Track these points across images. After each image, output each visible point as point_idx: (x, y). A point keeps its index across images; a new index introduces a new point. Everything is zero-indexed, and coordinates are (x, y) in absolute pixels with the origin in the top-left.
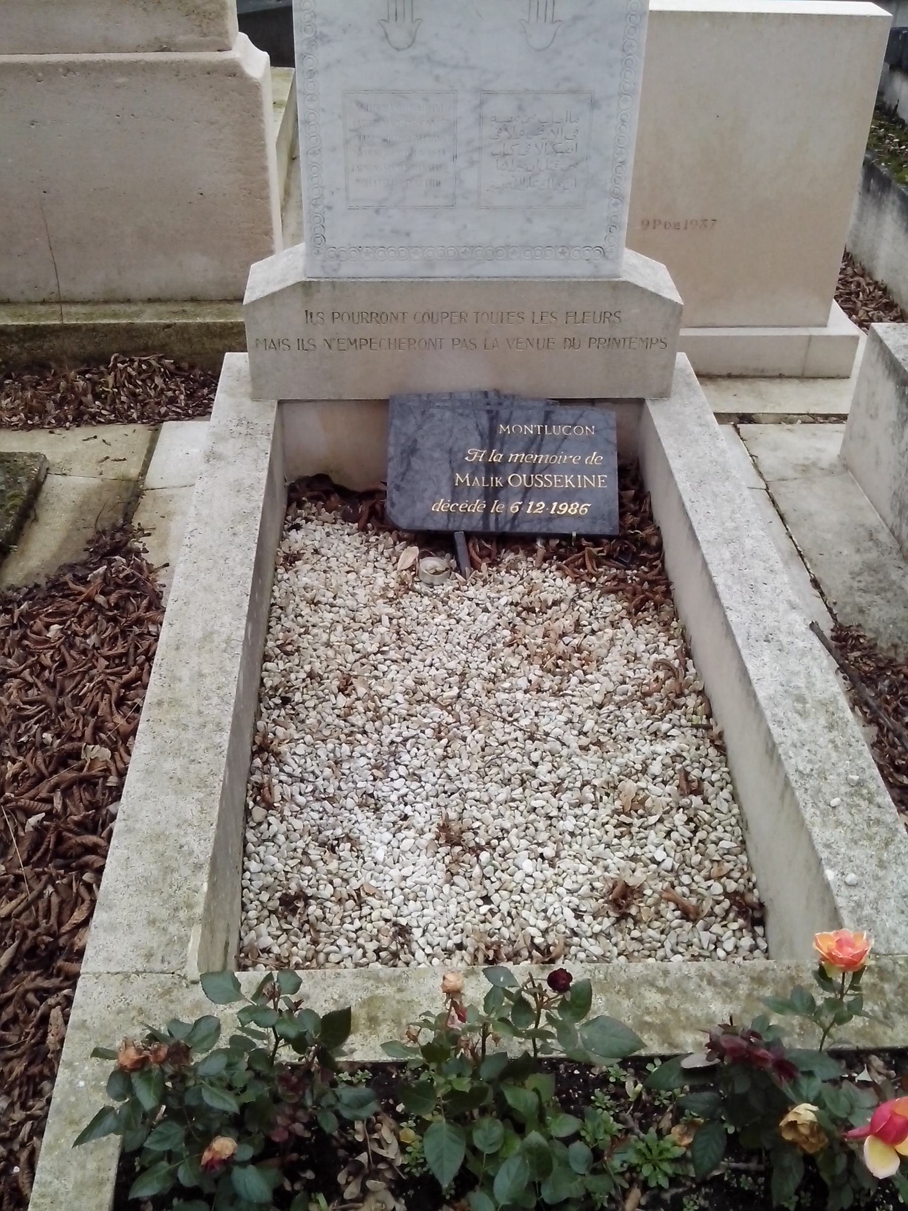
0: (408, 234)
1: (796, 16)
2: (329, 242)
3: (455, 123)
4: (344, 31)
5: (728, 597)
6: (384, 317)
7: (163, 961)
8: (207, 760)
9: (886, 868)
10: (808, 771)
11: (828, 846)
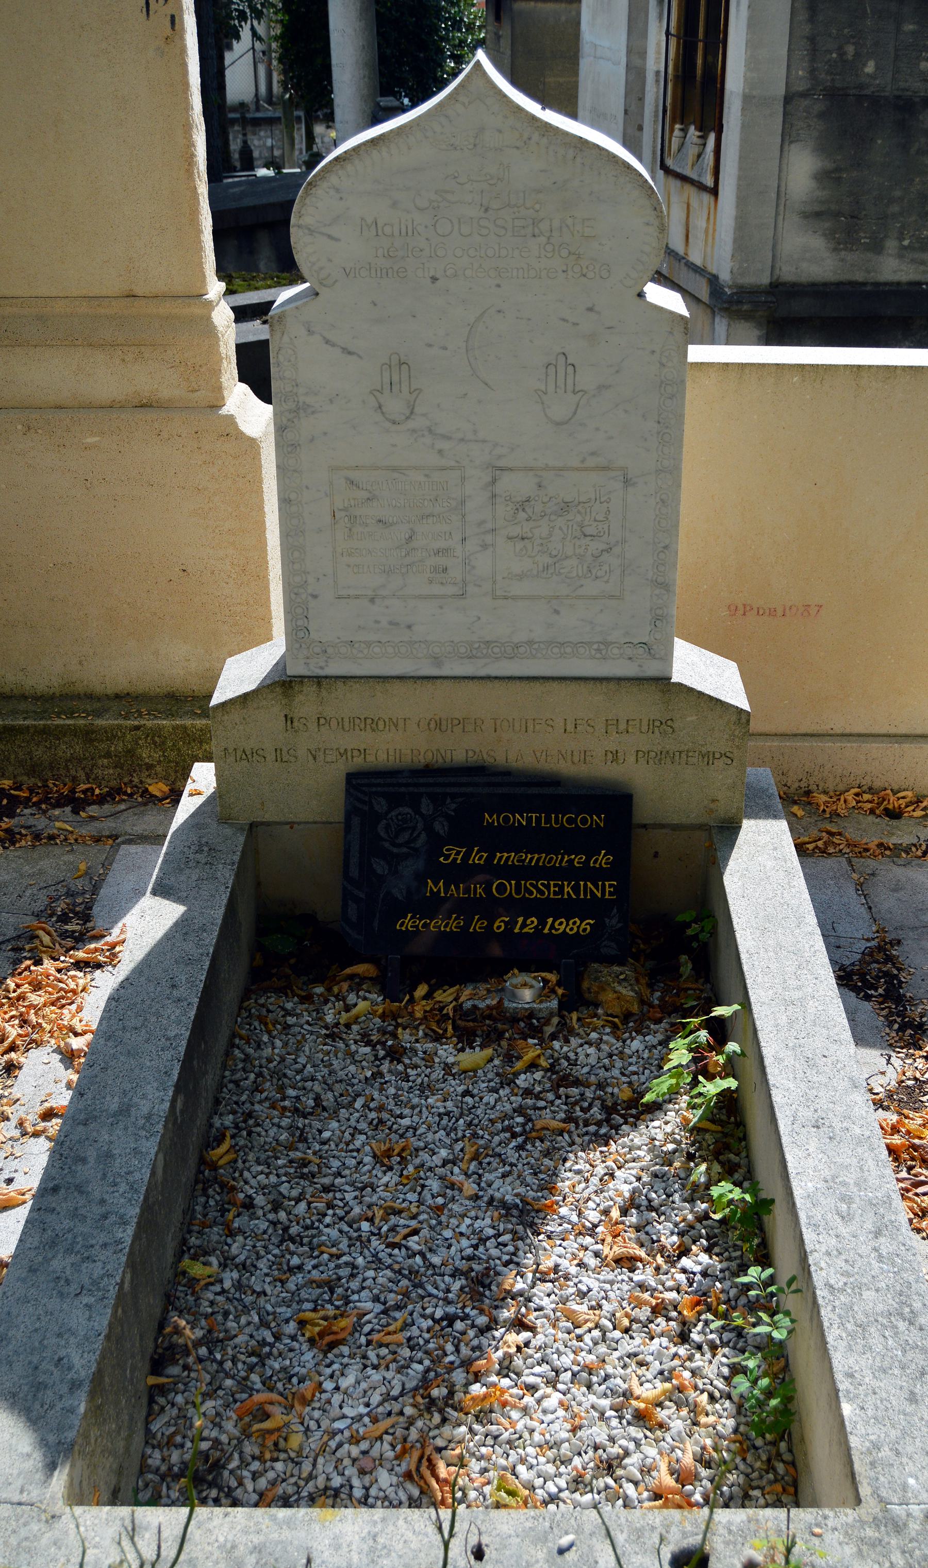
0: (409, 627)
1: (904, 368)
2: (314, 635)
3: (463, 502)
4: (331, 401)
5: (777, 1071)
6: (381, 723)
7: (22, 1492)
8: (102, 1258)
9: (916, 1402)
10: (841, 1284)
11: (850, 1375)
